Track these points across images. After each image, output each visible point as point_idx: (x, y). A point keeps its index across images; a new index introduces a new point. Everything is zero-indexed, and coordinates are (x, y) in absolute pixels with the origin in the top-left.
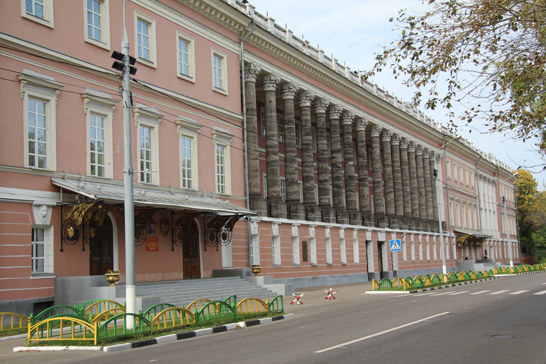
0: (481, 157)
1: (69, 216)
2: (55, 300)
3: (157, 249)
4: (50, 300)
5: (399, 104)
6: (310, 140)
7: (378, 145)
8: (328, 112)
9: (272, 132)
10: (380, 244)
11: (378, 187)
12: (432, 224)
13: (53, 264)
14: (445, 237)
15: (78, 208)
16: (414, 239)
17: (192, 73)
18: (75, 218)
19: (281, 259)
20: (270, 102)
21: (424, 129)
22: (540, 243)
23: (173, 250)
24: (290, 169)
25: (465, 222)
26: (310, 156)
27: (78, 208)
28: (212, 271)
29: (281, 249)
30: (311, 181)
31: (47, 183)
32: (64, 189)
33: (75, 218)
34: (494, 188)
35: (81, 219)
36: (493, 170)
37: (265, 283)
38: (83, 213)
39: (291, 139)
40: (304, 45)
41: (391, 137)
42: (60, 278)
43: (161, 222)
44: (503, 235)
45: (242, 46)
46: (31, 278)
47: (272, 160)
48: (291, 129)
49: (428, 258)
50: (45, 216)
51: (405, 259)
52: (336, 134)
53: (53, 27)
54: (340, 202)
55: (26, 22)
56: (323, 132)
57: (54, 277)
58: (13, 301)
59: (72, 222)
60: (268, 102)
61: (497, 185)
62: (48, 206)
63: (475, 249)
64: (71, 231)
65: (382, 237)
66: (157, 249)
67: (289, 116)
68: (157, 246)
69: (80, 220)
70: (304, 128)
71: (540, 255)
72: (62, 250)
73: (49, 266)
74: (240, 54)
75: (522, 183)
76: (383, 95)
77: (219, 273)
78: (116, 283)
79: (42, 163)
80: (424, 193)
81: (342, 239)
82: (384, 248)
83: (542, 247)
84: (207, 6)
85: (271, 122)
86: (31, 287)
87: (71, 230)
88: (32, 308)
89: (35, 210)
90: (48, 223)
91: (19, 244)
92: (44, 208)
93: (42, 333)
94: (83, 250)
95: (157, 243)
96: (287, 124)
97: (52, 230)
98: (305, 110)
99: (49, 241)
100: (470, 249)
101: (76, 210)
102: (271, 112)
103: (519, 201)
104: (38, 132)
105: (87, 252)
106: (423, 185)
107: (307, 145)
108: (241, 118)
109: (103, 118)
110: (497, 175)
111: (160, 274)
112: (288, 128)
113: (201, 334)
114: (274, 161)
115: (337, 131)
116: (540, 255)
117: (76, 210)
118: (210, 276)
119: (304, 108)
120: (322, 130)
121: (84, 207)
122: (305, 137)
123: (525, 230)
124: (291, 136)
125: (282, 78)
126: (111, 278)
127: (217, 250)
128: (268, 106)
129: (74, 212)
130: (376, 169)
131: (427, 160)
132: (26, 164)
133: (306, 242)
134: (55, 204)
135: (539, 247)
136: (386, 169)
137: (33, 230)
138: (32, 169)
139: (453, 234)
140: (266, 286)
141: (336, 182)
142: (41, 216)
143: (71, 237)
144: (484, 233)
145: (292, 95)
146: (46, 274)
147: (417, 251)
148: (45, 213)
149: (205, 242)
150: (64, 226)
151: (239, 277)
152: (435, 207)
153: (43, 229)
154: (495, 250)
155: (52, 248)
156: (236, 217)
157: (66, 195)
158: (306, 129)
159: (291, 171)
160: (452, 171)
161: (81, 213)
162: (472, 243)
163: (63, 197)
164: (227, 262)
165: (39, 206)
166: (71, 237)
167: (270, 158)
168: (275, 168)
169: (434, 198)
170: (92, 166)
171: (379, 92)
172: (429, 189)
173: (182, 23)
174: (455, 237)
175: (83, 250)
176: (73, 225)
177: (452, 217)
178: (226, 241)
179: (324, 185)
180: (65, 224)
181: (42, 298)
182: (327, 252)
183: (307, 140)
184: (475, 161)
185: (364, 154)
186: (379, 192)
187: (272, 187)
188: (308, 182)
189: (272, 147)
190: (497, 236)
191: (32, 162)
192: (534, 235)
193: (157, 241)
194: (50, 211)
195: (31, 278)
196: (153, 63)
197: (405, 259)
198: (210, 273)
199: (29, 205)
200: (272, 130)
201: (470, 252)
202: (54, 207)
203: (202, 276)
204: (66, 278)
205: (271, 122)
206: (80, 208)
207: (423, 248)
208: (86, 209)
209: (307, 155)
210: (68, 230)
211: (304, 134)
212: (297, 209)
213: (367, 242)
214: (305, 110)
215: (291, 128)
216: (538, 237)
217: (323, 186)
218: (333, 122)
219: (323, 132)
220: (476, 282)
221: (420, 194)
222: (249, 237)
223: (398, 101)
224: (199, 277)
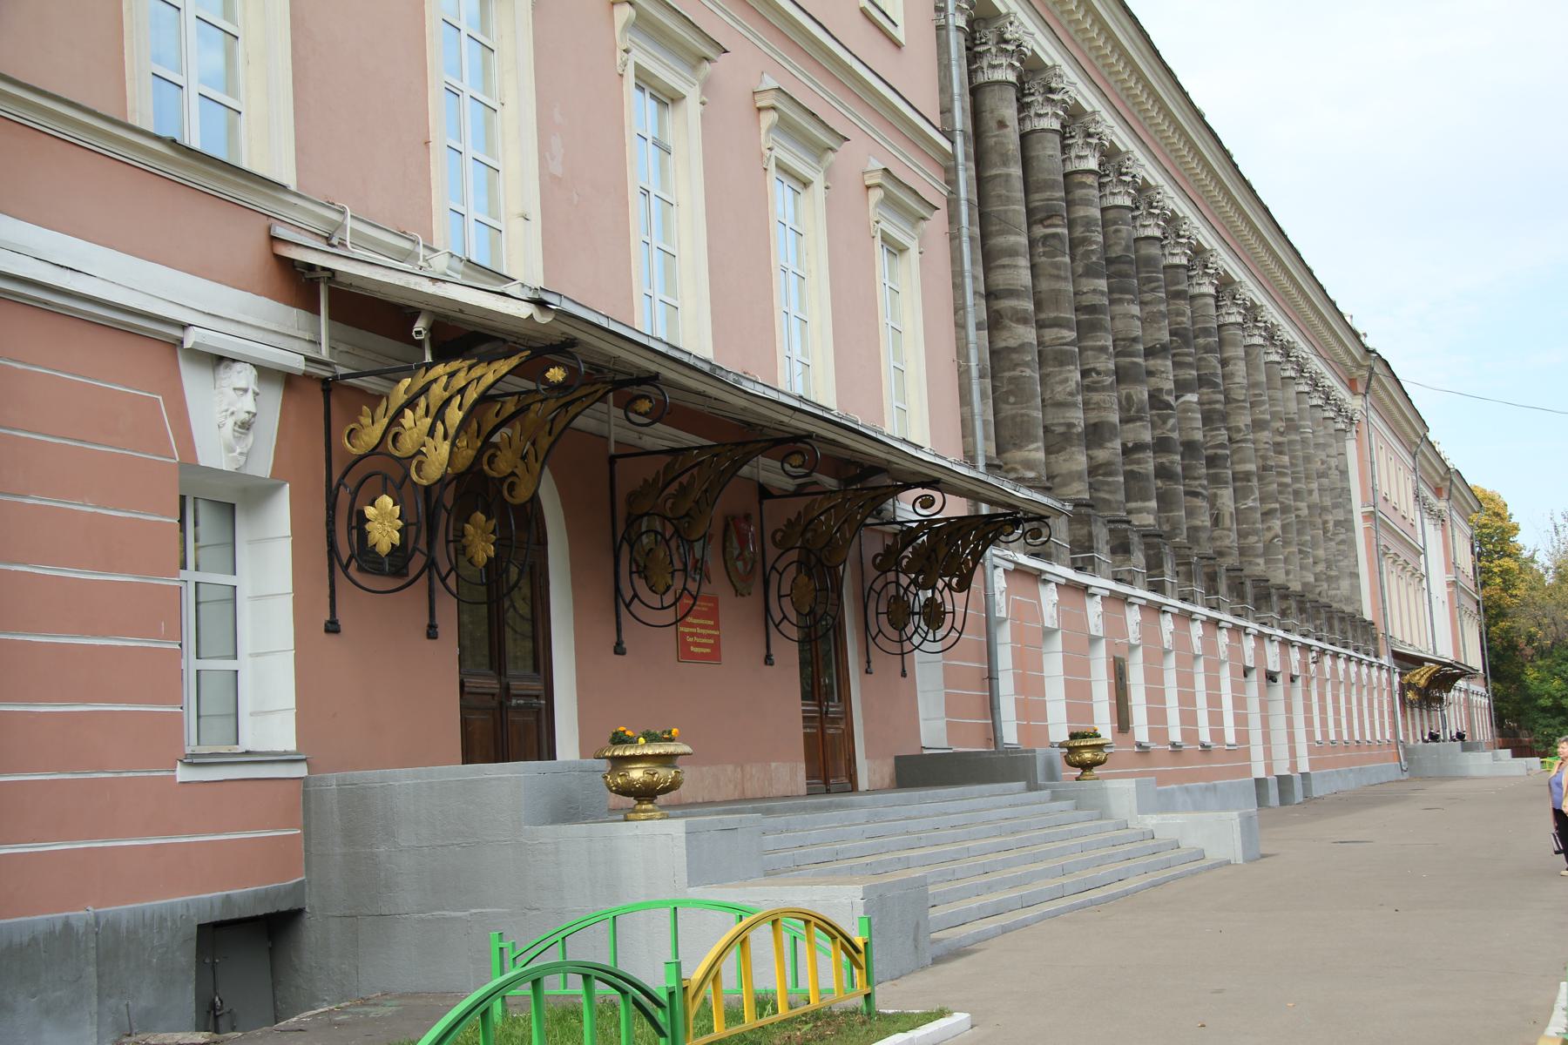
1: (372, 433)
2: (310, 903)
3: (714, 655)
4: (284, 906)
6: (1102, 293)
9: (1012, 239)
10: (1271, 677)
13: (291, 702)
15: (425, 390)
18: (407, 444)
20: (1002, 124)
22: (1550, 696)
24: (1059, 388)
26: (1103, 349)
27: (425, 390)
28: (891, 761)
29: (1066, 681)
30: (1110, 440)
31: (249, 250)
33: (407, 444)
35: (445, 448)
37: (1142, 810)
38: (455, 416)
39: (1058, 277)
42: (332, 779)
43: (727, 526)
46: (183, 774)
47: (1012, 343)
48: (1055, 242)
49: (1332, 737)
50: (245, 426)
52: (1153, 290)
56: (1127, 276)
57: (300, 771)
58: (81, 915)
59: (387, 469)
60: (993, 124)
61: (1448, 523)
62: (265, 373)
63: (1429, 706)
64: (384, 521)
65: (1273, 664)
66: (714, 655)
67: (1047, 194)
68: (717, 638)
70: (1081, 250)
71: (1550, 731)
72: (332, 627)
73: (270, 717)
75: (1485, 526)
77: (918, 771)
78: (661, 799)
81: (1196, 657)
83: (1557, 709)
85: (1008, 200)
86: (180, 833)
87: (383, 514)
88: (185, 958)
89: (193, 381)
90: (262, 467)
91: (110, 569)
92: (244, 376)
94: (432, 632)
95: (716, 627)
96: (1041, 221)
97: (280, 513)
98: (1083, 185)
99: (268, 567)
100: (1421, 709)
101: (411, 404)
102: (1005, 163)
103: (1483, 576)
105: (447, 650)
107: (1092, 309)
110: (1445, 496)
111: (730, 768)
112: (1046, 237)
114: (1021, 348)
115: (1158, 280)
116: (1550, 731)
117: (411, 404)
118: (887, 781)
119: (1079, 178)
120: (1125, 267)
121: (460, 381)
122: (1083, 280)
123: (1502, 660)
124: (1057, 266)
126: (637, 774)
127: (904, 674)
128: (992, 141)
129: (400, 413)
130: (1239, 430)
133: (1123, 660)
134: (297, 363)
135: (1544, 710)
137: (183, 498)
140: (1151, 821)
142: (228, 423)
143: (384, 548)
145: (1056, 115)
146: (252, 758)
148: (248, 403)
149: (868, 636)
150: (344, 497)
151: (1023, 784)
153: (229, 503)
155: (287, 604)
158: (1088, 254)
159: (1060, 397)
161: (440, 415)
163: (331, 338)
164: (933, 732)
165: (219, 360)
166: (384, 548)
167: (1005, 334)
168: (1028, 372)
175: (432, 632)
176: (399, 486)
178: (940, 633)
179: (1138, 462)
180: (352, 481)
181: (244, 893)
183: (1094, 291)
185: (1215, 375)
186: (1250, 508)
187: (1019, 447)
188: (1101, 446)
189: (1012, 293)
192: (1531, 675)
193: (713, 614)
194: (274, 398)
195: (183, 774)
197: (1318, 737)
198: (887, 769)
199: (160, 343)
200: (1009, 232)
202: (289, 381)
203: (863, 782)
204: (371, 775)
205: (1008, 200)
206: (437, 391)
208: (472, 395)
209: (1093, 348)
210: (370, 511)
211: (1080, 270)
212: (1090, 534)
213: (1247, 672)
214: (1083, 185)
215: (1055, 235)
216: (1542, 681)
217: (1135, 467)
219: (1127, 276)
222: (990, 626)
224: (853, 787)
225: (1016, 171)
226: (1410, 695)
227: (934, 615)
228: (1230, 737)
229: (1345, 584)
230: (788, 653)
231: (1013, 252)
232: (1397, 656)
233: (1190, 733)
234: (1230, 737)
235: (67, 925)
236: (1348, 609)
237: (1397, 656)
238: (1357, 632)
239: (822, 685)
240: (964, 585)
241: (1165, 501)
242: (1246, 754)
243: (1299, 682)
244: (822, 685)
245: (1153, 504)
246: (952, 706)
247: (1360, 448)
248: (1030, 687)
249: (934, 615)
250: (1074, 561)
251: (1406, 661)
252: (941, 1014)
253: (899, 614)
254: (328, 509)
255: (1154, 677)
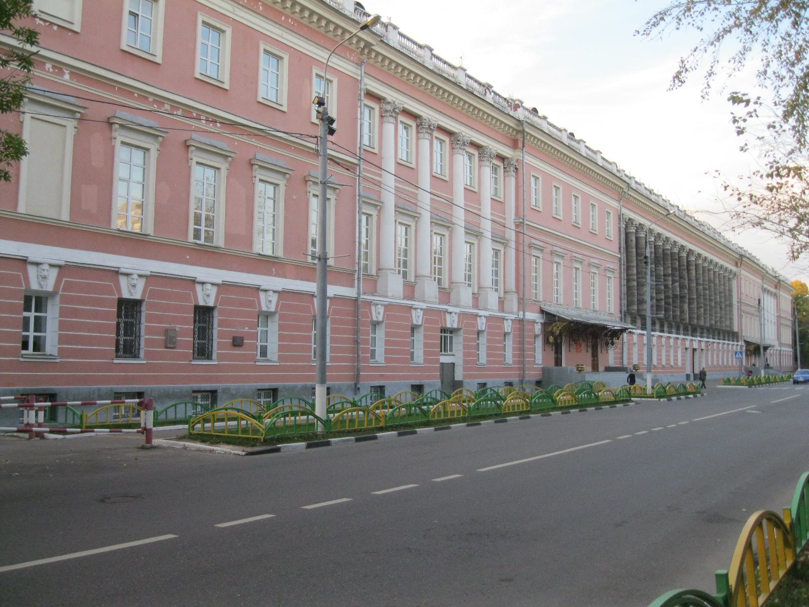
0: (767, 272)
1: (550, 329)
5: (665, 203)
7: (694, 268)
8: (688, 255)
10: (694, 350)
11: (693, 303)
12: (733, 335)
14: (737, 345)
16: (657, 341)
17: (284, 101)
18: (554, 331)
19: (279, 351)
20: (632, 241)
21: (725, 249)
23: (570, 351)
25: (751, 333)
31: (538, 309)
32: (546, 312)
34: (775, 300)
36: (736, 260)
38: (560, 328)
40: (650, 192)
41: (626, 222)
44: (781, 344)
45: (363, 69)
49: (725, 364)
51: (710, 364)
53: (286, 110)
54: (669, 316)
55: (261, 106)
59: (552, 333)
65: (695, 345)
69: (558, 332)
74: (359, 78)
76: (697, 224)
77: (608, 369)
79: (209, 238)
80: (723, 307)
82: (697, 354)
84: (303, 8)
93: (285, 419)
99: (539, 343)
100: (755, 356)
104: (206, 201)
106: (723, 300)
108: (619, 256)
109: (275, 188)
113: (336, 443)
125: (369, 87)
131: (728, 277)
132: (191, 238)
136: (698, 287)
138: (196, 244)
139: (743, 344)
141: (668, 300)
142: (538, 328)
144: (768, 342)
147: (659, 355)
152: (731, 319)
154: (707, 357)
156: (623, 330)
157: (548, 316)
160: (747, 287)
162: (755, 349)
164: (612, 363)
165: (537, 323)
169: (731, 311)
170: (441, 276)
171: (696, 222)
172: (728, 303)
173: (248, 20)
174: (745, 345)
177: (743, 328)
182: (485, 346)
184: (762, 276)
189: (632, 275)
190: (776, 343)
191: (197, 235)
195: (21, 359)
196: (223, 83)
201: (755, 359)
207: (666, 351)
213: (686, 349)
218: (666, 252)
220: (695, 396)
221: (721, 308)
223: (663, 200)
225: (634, 250)
226: (748, 353)
227: (613, 344)
228: (680, 363)
229: (728, 323)
230: (590, 350)
231: (633, 267)
232: (745, 341)
233: (718, 364)
234: (680, 363)
235: (324, 439)
236: (728, 329)
237: (745, 341)
238: (733, 335)
239: (595, 355)
240: (618, 339)
241: (666, 310)
242: (684, 368)
243: (704, 351)
244: (595, 355)
245: (663, 312)
246: (615, 358)
247: (737, 282)
248: (630, 354)
249: (613, 344)
250: (642, 328)
251: (748, 343)
252: (535, 194)
253: (607, 344)
254: (620, 371)
255: (659, 351)
